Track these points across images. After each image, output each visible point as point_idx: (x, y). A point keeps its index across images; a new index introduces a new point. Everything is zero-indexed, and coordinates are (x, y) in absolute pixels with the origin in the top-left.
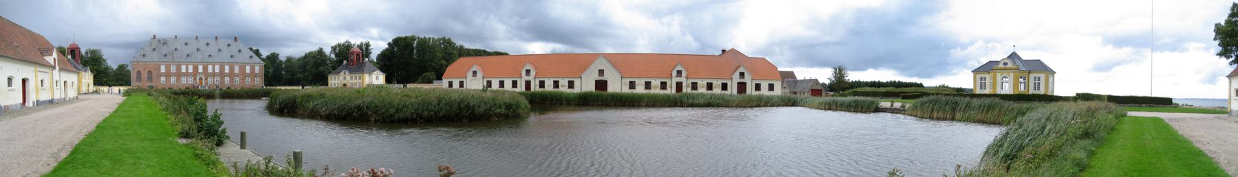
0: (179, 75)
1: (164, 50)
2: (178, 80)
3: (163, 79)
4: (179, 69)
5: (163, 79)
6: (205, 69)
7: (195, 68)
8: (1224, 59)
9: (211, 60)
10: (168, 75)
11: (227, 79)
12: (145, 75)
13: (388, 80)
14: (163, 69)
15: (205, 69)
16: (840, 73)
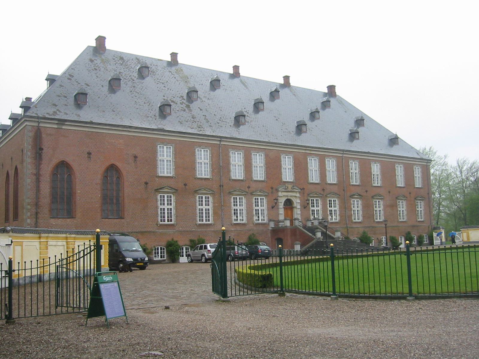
2: (221, 209)
3: (167, 205)
5: (167, 205)
6: (300, 168)
7: (273, 167)
9: (356, 146)
11: (357, 206)
15: (300, 168)
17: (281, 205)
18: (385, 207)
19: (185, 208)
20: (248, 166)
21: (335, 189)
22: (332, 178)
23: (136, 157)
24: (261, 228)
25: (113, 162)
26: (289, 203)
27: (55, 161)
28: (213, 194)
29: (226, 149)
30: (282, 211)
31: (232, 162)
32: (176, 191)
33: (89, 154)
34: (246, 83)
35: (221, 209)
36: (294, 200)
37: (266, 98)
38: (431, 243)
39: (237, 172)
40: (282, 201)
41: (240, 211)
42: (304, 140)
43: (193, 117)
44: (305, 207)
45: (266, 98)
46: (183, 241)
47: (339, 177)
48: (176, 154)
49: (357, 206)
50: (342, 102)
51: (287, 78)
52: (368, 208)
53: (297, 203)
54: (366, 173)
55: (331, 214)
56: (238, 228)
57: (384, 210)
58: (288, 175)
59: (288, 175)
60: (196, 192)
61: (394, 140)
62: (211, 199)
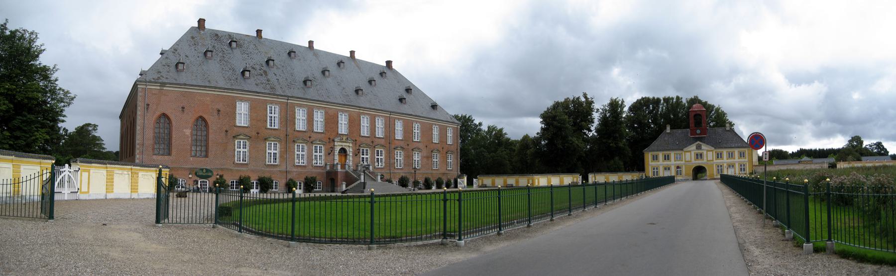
0: (288, 137)
1: (238, 61)
2: (286, 153)
3: (242, 150)
4: (288, 119)
5: (242, 150)
6: (354, 124)
7: (331, 122)
8: (13, 30)
9: (405, 108)
10: (257, 135)
11: (399, 156)
12: (183, 132)
13: (261, 192)
14: (242, 113)
15: (354, 124)
16: (857, 140)
17: (337, 153)
18: (423, 157)
19: (257, 153)
20: (310, 120)
21: (383, 142)
22: (380, 133)
23: (219, 111)
24: (320, 171)
25: (201, 114)
26: (343, 151)
27: (158, 113)
28: (280, 141)
29: (293, 107)
30: (337, 157)
31: (297, 117)
32: (250, 138)
33: (183, 108)
34: (317, 54)
35: (286, 153)
36: (347, 149)
37: (376, 77)
38: (456, 187)
39: (301, 124)
40: (337, 149)
41: (301, 155)
42: (362, 101)
43: (268, 80)
44: (356, 154)
45: (376, 77)
46: (432, 180)
47: (386, 132)
48: (252, 109)
49: (399, 156)
50: (396, 73)
51: (352, 53)
52: (408, 157)
53: (350, 151)
54: (408, 131)
55: (316, 159)
56: (300, 170)
57: (422, 160)
58: (343, 128)
59: (343, 128)
60: (266, 139)
61: (434, 106)
62: (278, 145)
